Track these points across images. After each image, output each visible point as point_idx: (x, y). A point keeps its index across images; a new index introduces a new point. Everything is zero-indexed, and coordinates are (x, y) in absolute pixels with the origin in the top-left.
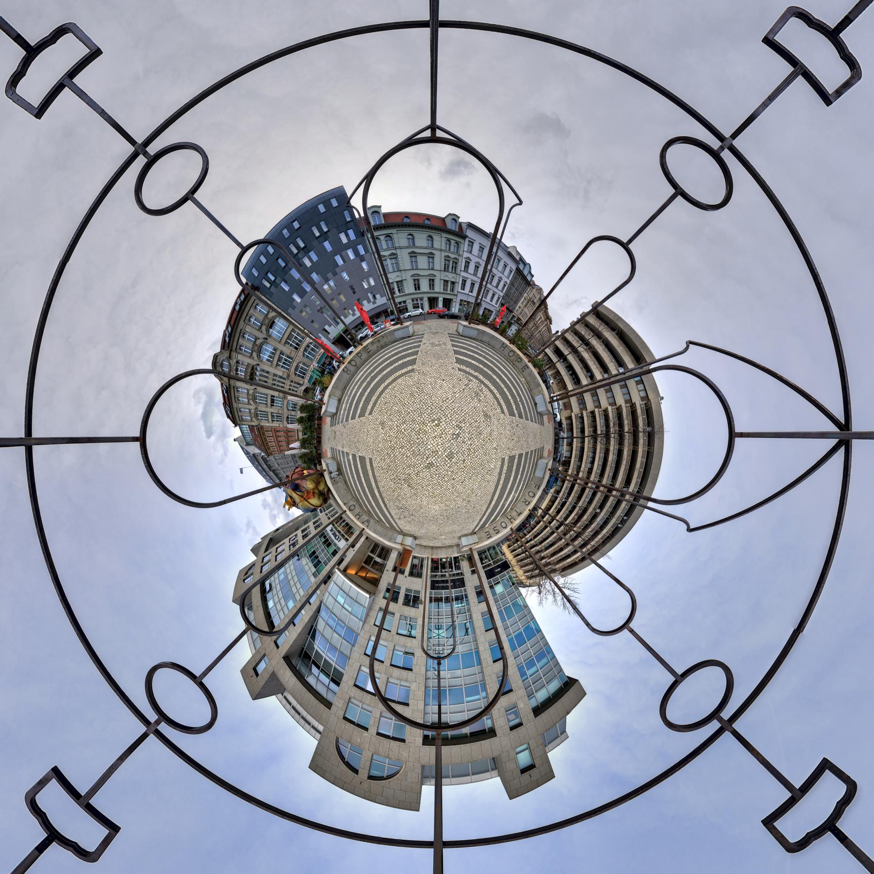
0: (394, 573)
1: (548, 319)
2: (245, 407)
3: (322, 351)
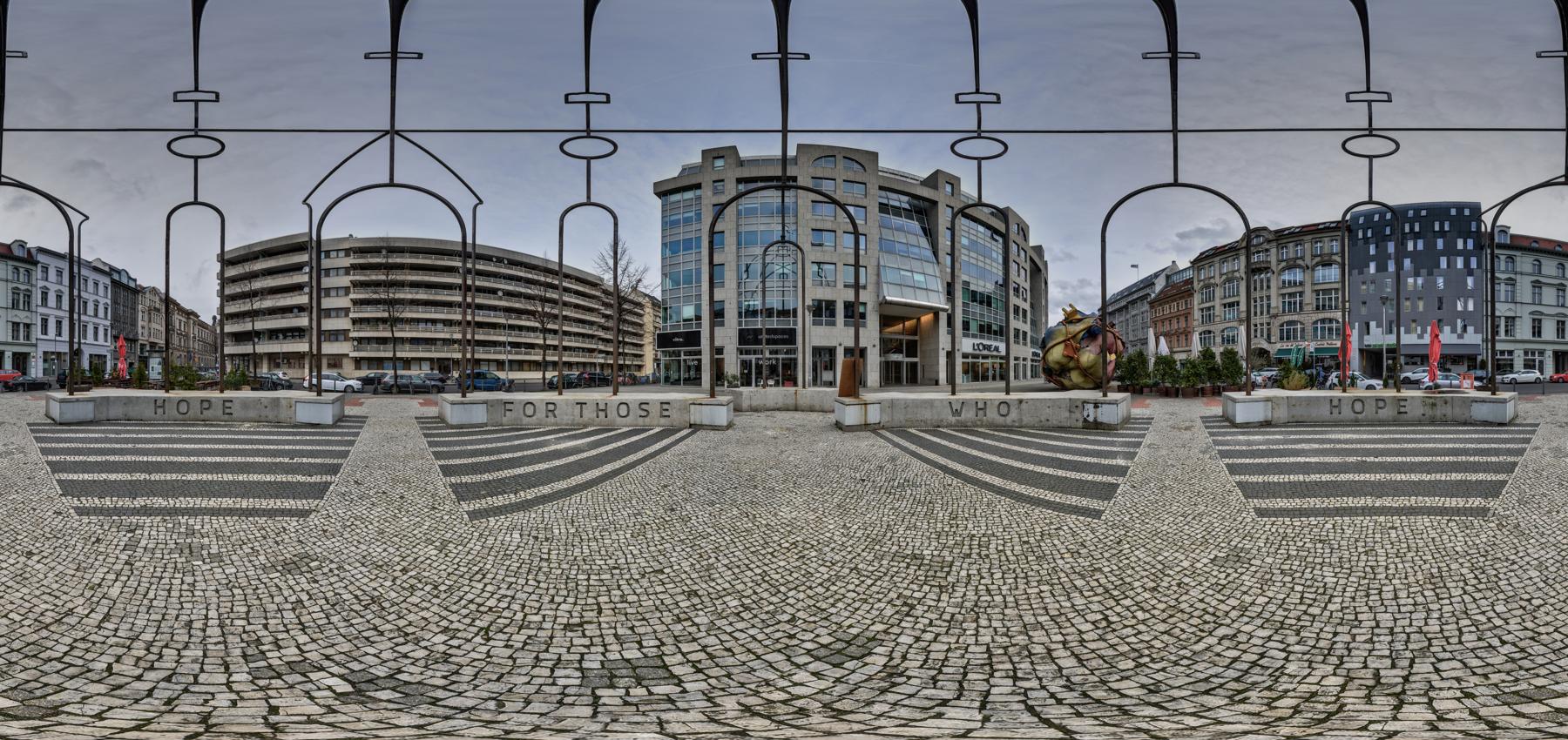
2: (1215, 272)
3: (1339, 344)
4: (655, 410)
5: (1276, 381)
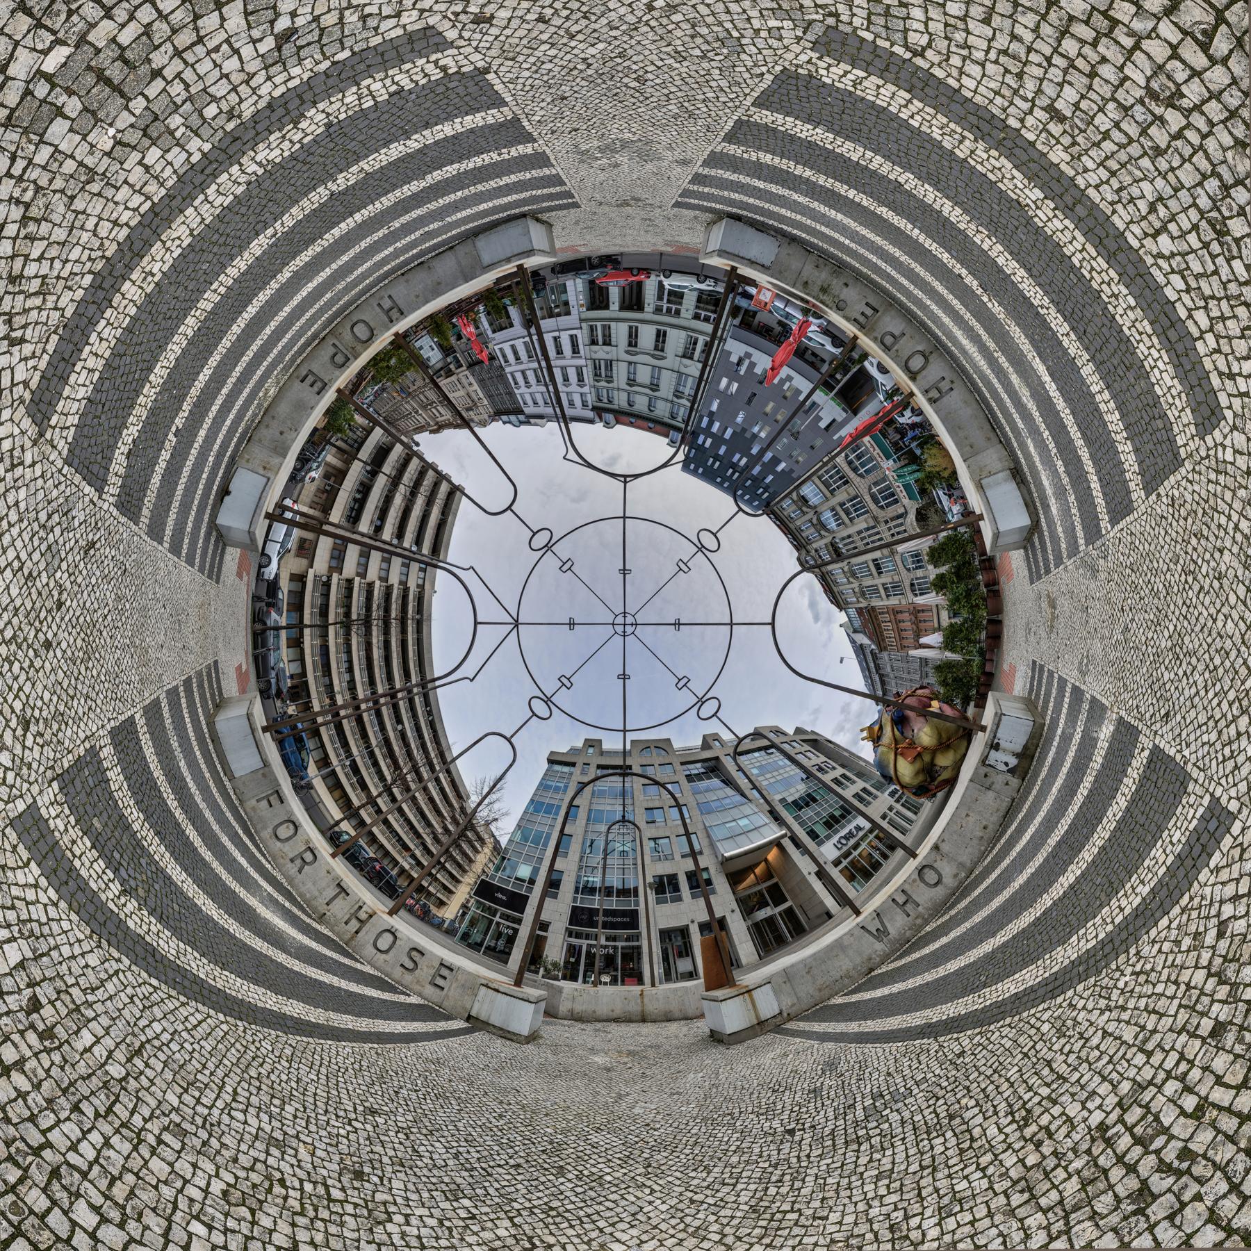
0: (718, 915)
1: (440, 428)
2: (847, 588)
3: (867, 439)
4: (425, 971)
5: (950, 487)
